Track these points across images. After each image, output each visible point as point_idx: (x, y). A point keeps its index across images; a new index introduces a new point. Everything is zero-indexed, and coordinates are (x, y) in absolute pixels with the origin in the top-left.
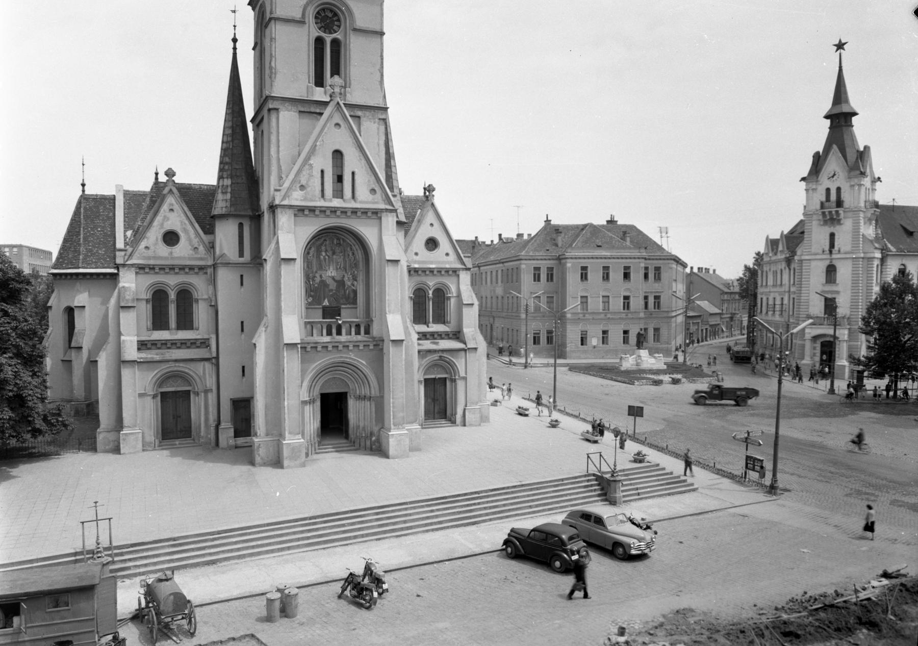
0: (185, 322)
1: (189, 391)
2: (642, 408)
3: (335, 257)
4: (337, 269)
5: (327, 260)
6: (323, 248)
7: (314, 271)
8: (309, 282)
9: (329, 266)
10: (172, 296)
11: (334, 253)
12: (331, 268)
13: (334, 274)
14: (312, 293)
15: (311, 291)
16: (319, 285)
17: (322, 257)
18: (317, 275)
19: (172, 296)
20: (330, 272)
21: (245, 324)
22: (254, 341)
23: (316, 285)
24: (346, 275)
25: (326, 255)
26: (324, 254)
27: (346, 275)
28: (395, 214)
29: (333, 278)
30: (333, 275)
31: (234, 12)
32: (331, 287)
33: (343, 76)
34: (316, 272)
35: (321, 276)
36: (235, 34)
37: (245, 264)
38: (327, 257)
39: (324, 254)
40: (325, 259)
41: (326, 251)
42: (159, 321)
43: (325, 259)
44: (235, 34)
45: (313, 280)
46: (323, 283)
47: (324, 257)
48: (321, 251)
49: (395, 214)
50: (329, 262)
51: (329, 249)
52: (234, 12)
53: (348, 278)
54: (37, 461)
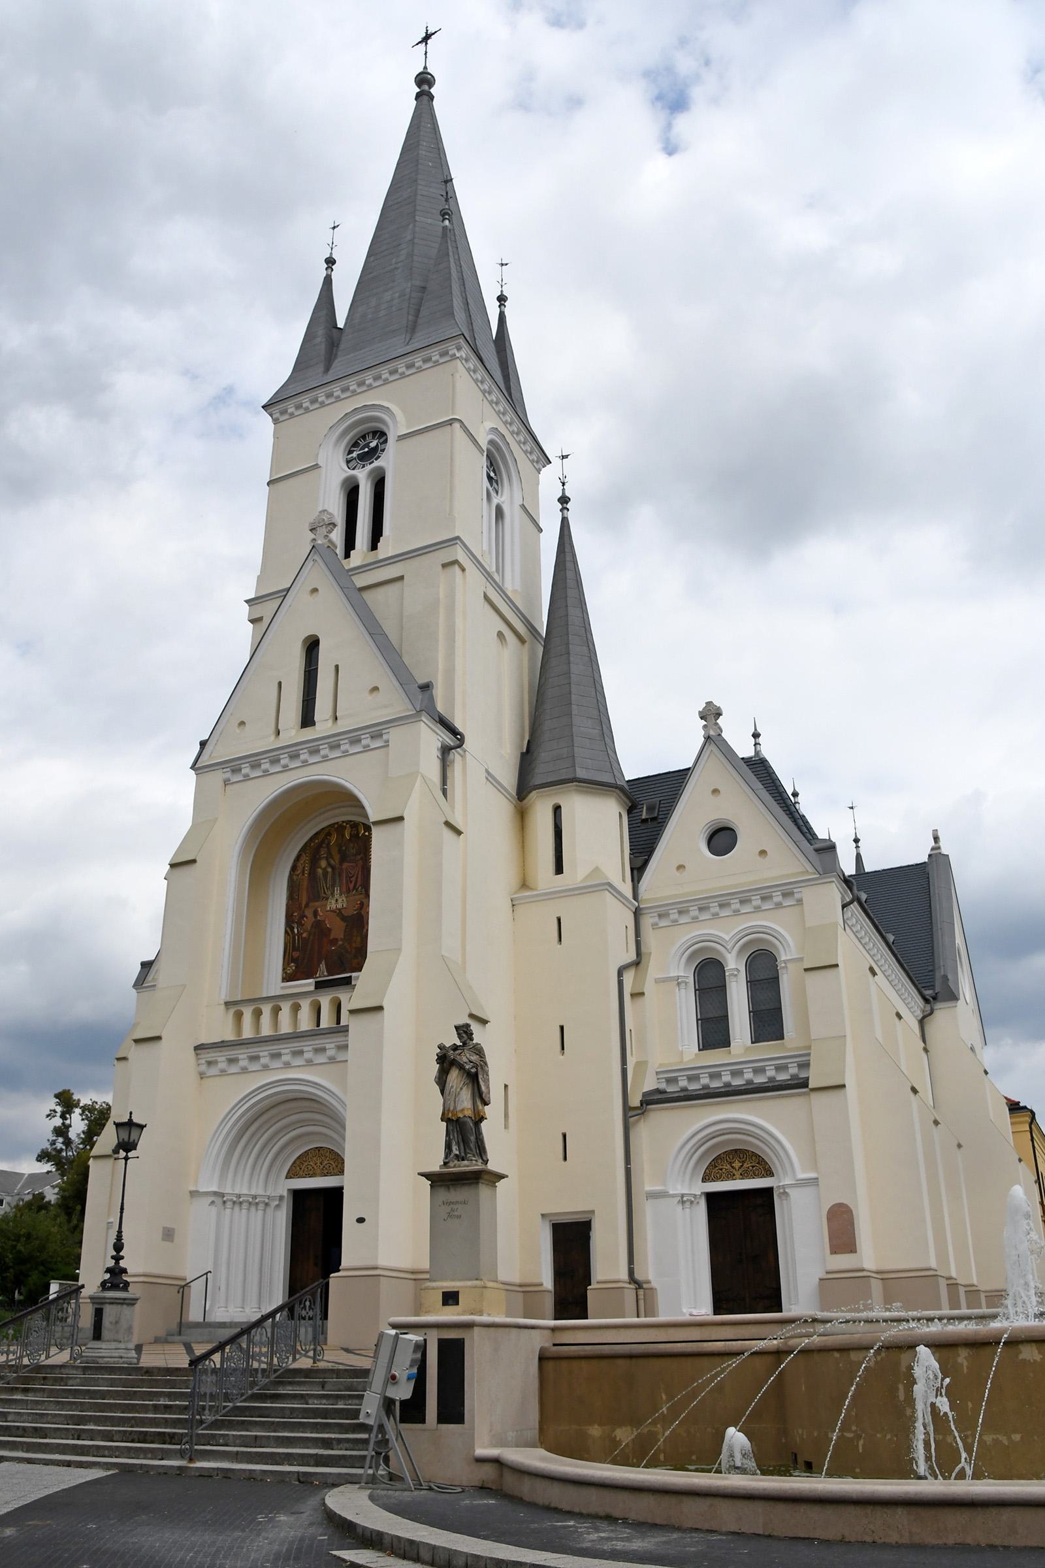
2: (444, 823)
3: (345, 865)
4: (348, 891)
5: (329, 876)
6: (323, 852)
7: (304, 903)
8: (292, 929)
9: (333, 886)
11: (343, 859)
12: (337, 891)
14: (296, 954)
15: (294, 949)
16: (310, 934)
17: (320, 871)
18: (309, 913)
20: (333, 902)
21: (561, 1156)
22: (72, 1465)
23: (304, 935)
25: (329, 864)
28: (457, 567)
30: (339, 906)
31: (852, 808)
33: (292, 1299)
34: (307, 906)
35: (315, 913)
36: (856, 833)
37: (407, 1272)
38: (329, 870)
39: (323, 863)
40: (325, 874)
41: (330, 856)
44: (856, 833)
45: (300, 924)
46: (320, 929)
47: (324, 869)
48: (320, 859)
49: (457, 567)
51: (335, 852)
52: (852, 808)
54: (517, 777)
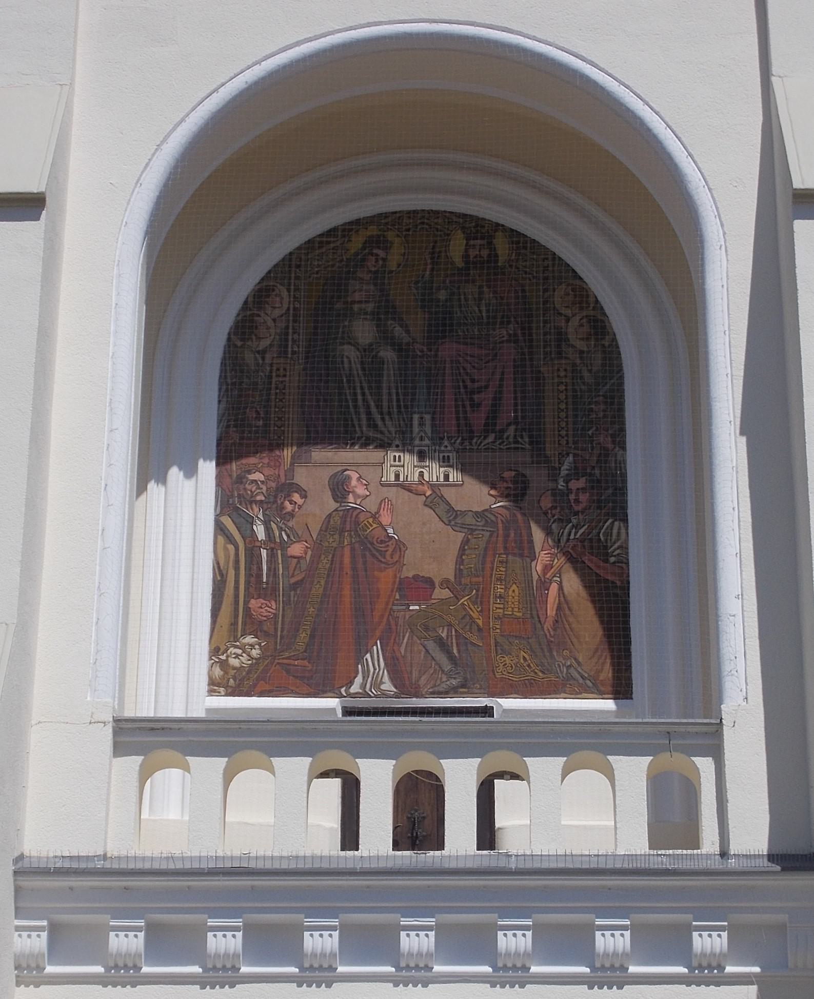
35: (339, 488)
38: (388, 354)
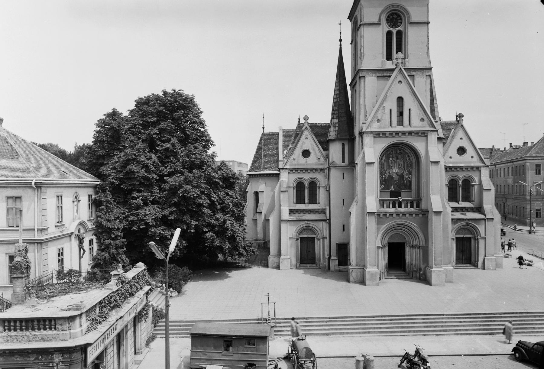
0: (313, 199)
1: (314, 238)
3: (398, 161)
6: (391, 156)
9: (394, 166)
10: (306, 185)
13: (397, 171)
17: (390, 161)
19: (306, 185)
24: (404, 171)
25: (393, 160)
26: (391, 159)
27: (404, 171)
29: (397, 174)
32: (395, 179)
35: (389, 173)
40: (392, 162)
42: (300, 199)
43: (392, 162)
47: (391, 161)
50: (394, 164)
51: (394, 156)
53: (406, 173)
